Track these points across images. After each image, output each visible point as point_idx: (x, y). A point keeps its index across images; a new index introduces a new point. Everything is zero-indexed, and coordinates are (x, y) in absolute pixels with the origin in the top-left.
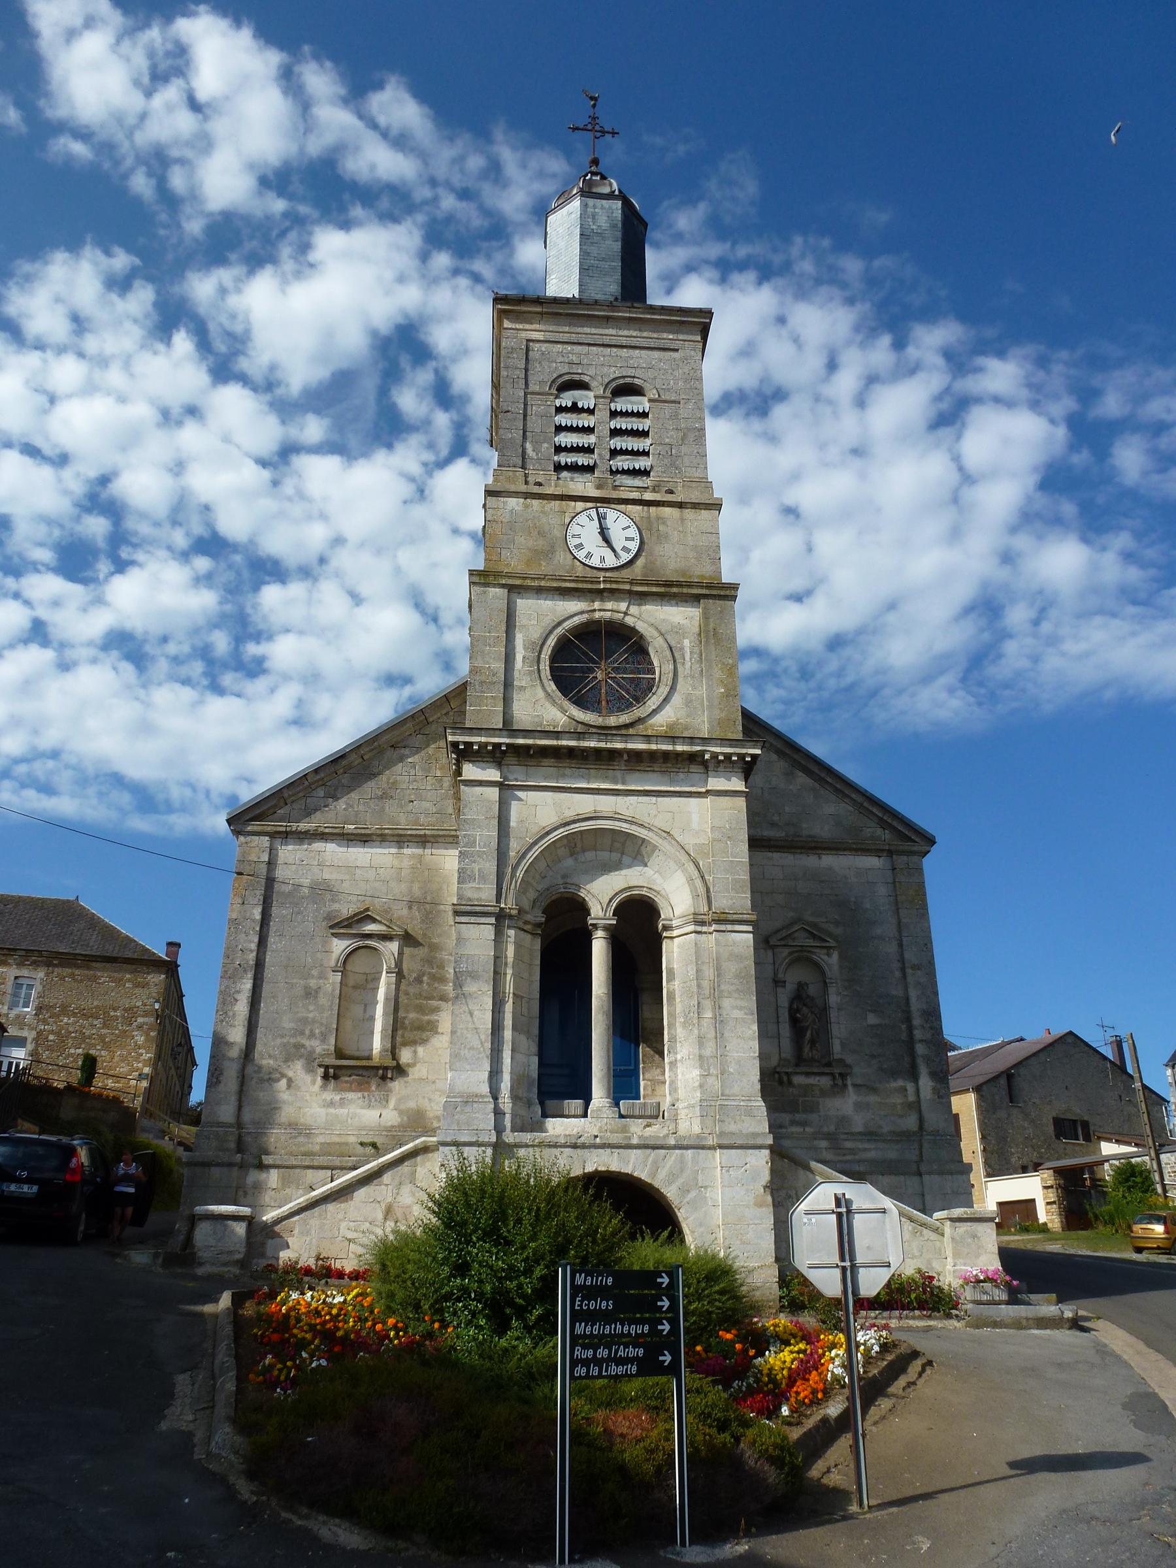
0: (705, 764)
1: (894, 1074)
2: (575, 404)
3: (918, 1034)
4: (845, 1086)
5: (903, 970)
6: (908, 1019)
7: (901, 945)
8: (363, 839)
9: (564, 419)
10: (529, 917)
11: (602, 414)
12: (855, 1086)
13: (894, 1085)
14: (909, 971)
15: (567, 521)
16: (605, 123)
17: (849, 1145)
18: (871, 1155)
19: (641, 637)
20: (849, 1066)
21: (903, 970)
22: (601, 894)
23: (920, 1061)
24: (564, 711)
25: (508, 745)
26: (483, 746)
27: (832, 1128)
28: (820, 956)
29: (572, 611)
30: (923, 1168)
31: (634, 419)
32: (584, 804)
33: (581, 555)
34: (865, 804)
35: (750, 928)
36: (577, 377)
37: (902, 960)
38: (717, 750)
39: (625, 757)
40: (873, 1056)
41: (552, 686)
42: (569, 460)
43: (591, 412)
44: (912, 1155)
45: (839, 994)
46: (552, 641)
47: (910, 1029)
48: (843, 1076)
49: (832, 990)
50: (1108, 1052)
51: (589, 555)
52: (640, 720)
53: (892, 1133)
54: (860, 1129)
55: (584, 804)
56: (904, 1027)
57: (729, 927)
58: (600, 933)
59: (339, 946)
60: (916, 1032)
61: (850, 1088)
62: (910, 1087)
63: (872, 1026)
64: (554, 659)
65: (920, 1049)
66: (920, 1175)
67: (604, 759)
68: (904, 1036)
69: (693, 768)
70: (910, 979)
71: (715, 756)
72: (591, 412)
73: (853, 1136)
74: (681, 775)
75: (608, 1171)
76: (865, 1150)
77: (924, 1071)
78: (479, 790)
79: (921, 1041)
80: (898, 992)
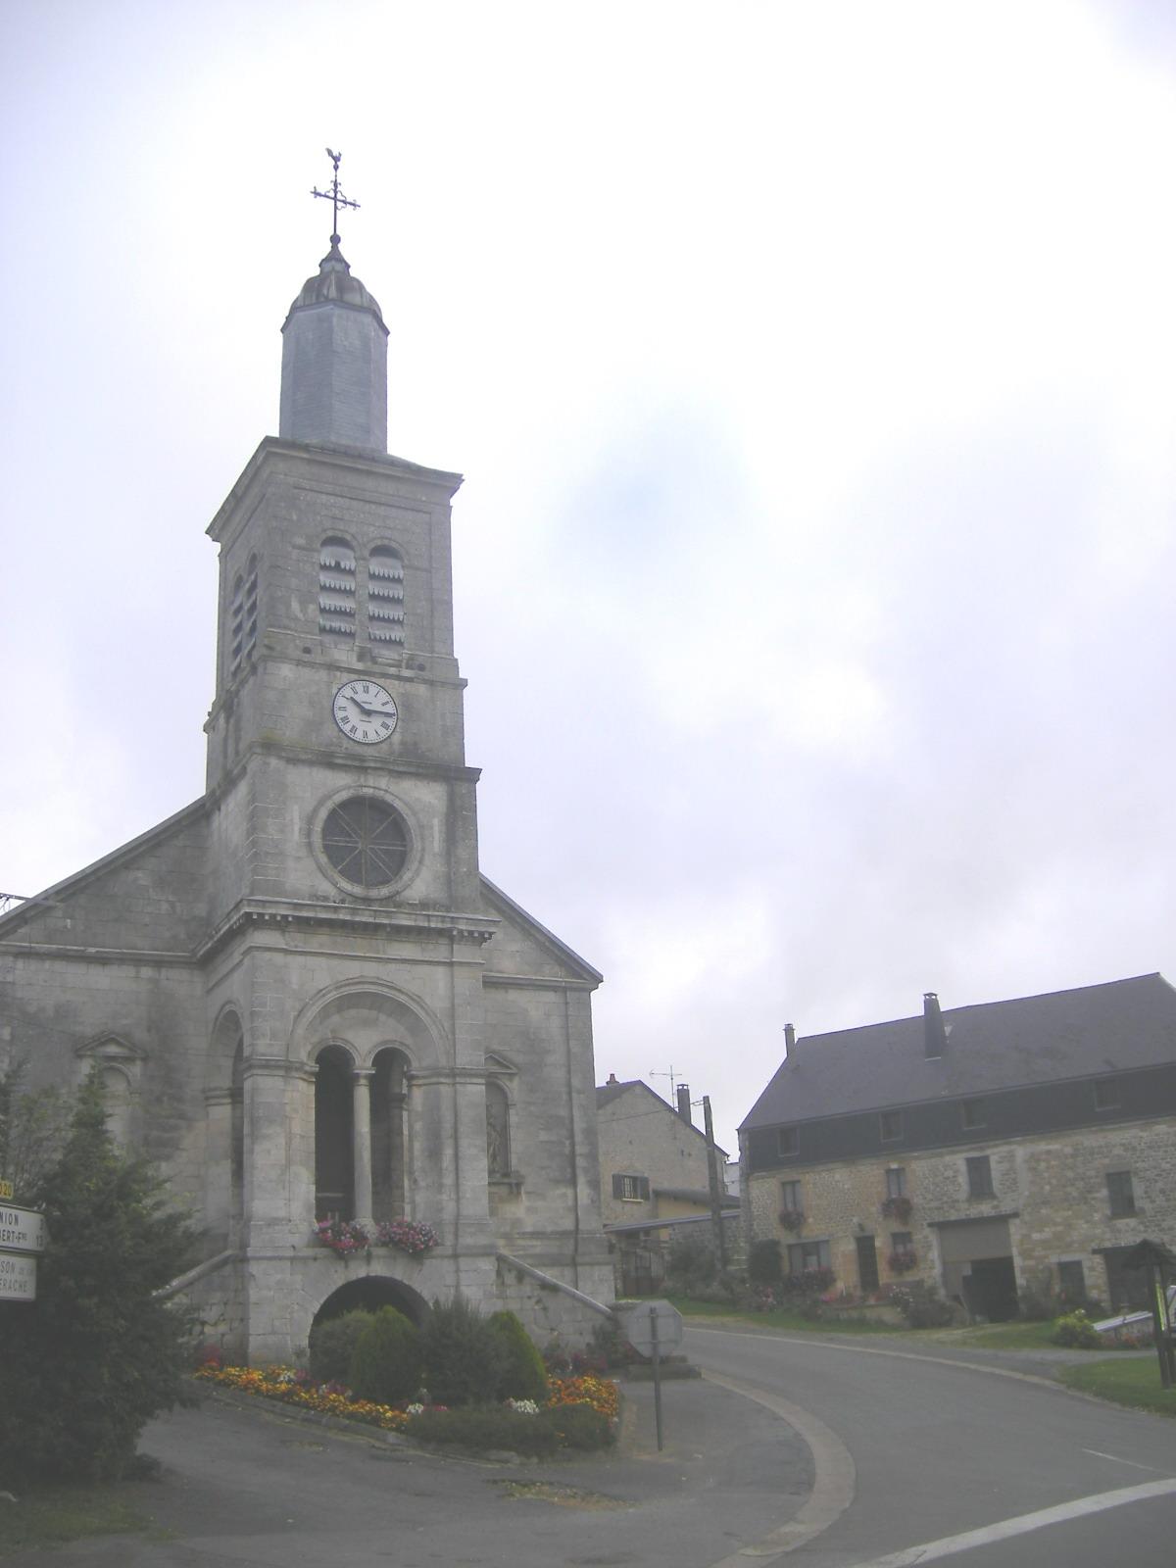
0: (452, 939)
1: (557, 1182)
2: (338, 564)
3: (579, 1149)
4: (519, 1193)
5: (570, 1093)
6: (572, 1136)
7: (569, 1072)
8: (103, 961)
9: (325, 579)
10: (307, 1068)
11: (362, 577)
12: (527, 1193)
13: (558, 1192)
14: (574, 1095)
15: (334, 691)
16: (347, 191)
17: (520, 1242)
18: (537, 1250)
19: (400, 814)
20: (523, 1177)
21: (570, 1093)
22: (363, 1044)
23: (579, 1172)
24: (335, 885)
25: (293, 917)
26: (273, 916)
27: (508, 1229)
28: (504, 1083)
29: (341, 785)
30: (579, 1259)
31: (391, 585)
32: (353, 970)
33: (347, 728)
34: (547, 944)
35: (483, 1081)
36: (339, 534)
37: (569, 1085)
38: (463, 927)
39: (388, 929)
40: (543, 1168)
41: (323, 859)
42: (333, 625)
43: (351, 573)
44: (568, 1249)
45: (517, 1114)
46: (323, 814)
47: (573, 1145)
48: (518, 1185)
49: (512, 1112)
50: (673, 1102)
51: (354, 729)
52: (398, 893)
53: (552, 1233)
54: (529, 1229)
55: (353, 970)
56: (567, 1142)
57: (468, 1080)
58: (363, 1081)
59: (85, 1067)
60: (577, 1147)
61: (524, 1196)
62: (570, 1192)
63: (542, 1142)
64: (326, 831)
65: (580, 1162)
66: (574, 1264)
67: (371, 930)
68: (567, 1151)
69: (442, 941)
70: (574, 1102)
71: (461, 932)
72: (351, 573)
73: (524, 1235)
74: (431, 947)
75: (376, 1276)
76: (532, 1246)
77: (581, 1180)
78: (267, 955)
79: (581, 1155)
80: (563, 1112)
